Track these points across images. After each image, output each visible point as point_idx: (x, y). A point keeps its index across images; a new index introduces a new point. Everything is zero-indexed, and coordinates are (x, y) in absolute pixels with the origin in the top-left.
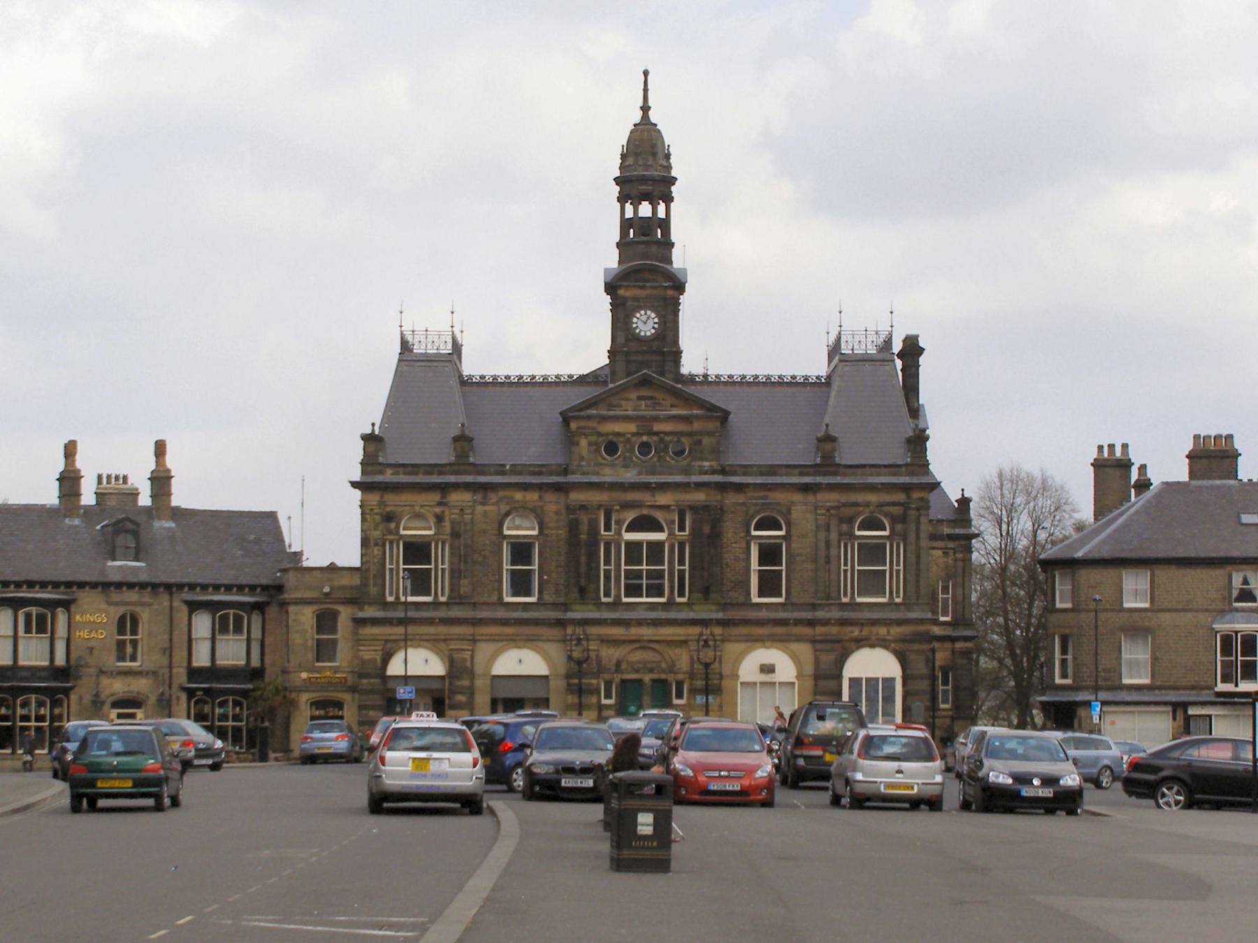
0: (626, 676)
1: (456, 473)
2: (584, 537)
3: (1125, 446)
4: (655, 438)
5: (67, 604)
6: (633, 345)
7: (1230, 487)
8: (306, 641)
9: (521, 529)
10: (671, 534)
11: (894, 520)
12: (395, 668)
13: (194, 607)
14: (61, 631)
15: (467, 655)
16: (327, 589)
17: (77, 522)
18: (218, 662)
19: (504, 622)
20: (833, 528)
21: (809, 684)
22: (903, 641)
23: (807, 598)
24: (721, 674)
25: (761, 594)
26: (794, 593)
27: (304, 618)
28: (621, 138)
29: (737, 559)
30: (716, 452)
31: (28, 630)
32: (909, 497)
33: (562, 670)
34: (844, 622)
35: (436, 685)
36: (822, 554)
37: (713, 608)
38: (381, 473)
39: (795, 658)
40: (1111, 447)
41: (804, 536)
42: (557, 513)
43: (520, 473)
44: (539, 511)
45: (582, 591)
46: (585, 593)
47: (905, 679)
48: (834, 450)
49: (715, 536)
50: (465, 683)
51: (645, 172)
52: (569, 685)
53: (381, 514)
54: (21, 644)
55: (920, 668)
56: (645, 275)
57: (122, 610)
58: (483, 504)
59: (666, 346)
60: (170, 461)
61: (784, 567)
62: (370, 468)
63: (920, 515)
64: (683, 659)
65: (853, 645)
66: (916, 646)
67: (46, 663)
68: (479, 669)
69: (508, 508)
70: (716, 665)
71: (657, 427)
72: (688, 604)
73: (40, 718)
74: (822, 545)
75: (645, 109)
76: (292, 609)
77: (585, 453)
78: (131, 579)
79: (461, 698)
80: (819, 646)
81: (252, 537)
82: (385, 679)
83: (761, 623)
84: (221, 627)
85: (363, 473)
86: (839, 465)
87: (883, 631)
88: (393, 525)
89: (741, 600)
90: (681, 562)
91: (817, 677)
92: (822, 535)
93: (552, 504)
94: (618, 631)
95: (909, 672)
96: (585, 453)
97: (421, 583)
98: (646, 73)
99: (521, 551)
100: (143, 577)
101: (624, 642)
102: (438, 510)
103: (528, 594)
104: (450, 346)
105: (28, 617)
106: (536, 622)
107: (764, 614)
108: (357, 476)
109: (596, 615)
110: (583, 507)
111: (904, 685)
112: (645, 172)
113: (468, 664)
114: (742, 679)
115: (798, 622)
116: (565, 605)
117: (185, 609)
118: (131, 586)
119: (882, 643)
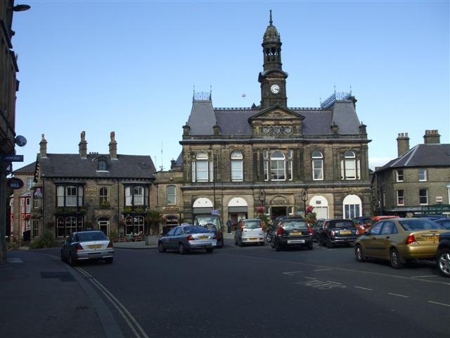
1: (215, 138)
2: (258, 159)
3: (406, 134)
5: (83, 185)
11: (357, 153)
12: (195, 205)
13: (126, 185)
14: (81, 194)
15: (220, 200)
17: (85, 158)
19: (233, 188)
21: (333, 207)
26: (430, 177)
29: (308, 166)
31: (69, 194)
33: (252, 204)
36: (335, 163)
38: (190, 138)
39: (327, 198)
40: (403, 134)
42: (249, 151)
43: (236, 138)
47: (363, 204)
49: (302, 158)
51: (272, 47)
52: (255, 209)
54: (67, 198)
55: (367, 200)
56: (273, 73)
57: (102, 187)
58: (224, 149)
59: (282, 97)
60: (116, 138)
64: (292, 199)
65: (345, 194)
66: (366, 194)
67: (76, 205)
68: (224, 205)
71: (281, 123)
73: (73, 225)
74: (335, 161)
75: (271, 22)
76: (159, 185)
77: (258, 131)
78: (104, 176)
82: (193, 208)
85: (183, 138)
87: (355, 189)
91: (335, 205)
93: (248, 148)
94: (271, 191)
96: (258, 131)
100: (109, 176)
101: (272, 194)
102: (209, 151)
103: (426, 202)
105: (69, 189)
107: (317, 184)
109: (263, 185)
111: (363, 207)
112: (272, 47)
117: (123, 186)
118: (104, 178)
119: (355, 193)
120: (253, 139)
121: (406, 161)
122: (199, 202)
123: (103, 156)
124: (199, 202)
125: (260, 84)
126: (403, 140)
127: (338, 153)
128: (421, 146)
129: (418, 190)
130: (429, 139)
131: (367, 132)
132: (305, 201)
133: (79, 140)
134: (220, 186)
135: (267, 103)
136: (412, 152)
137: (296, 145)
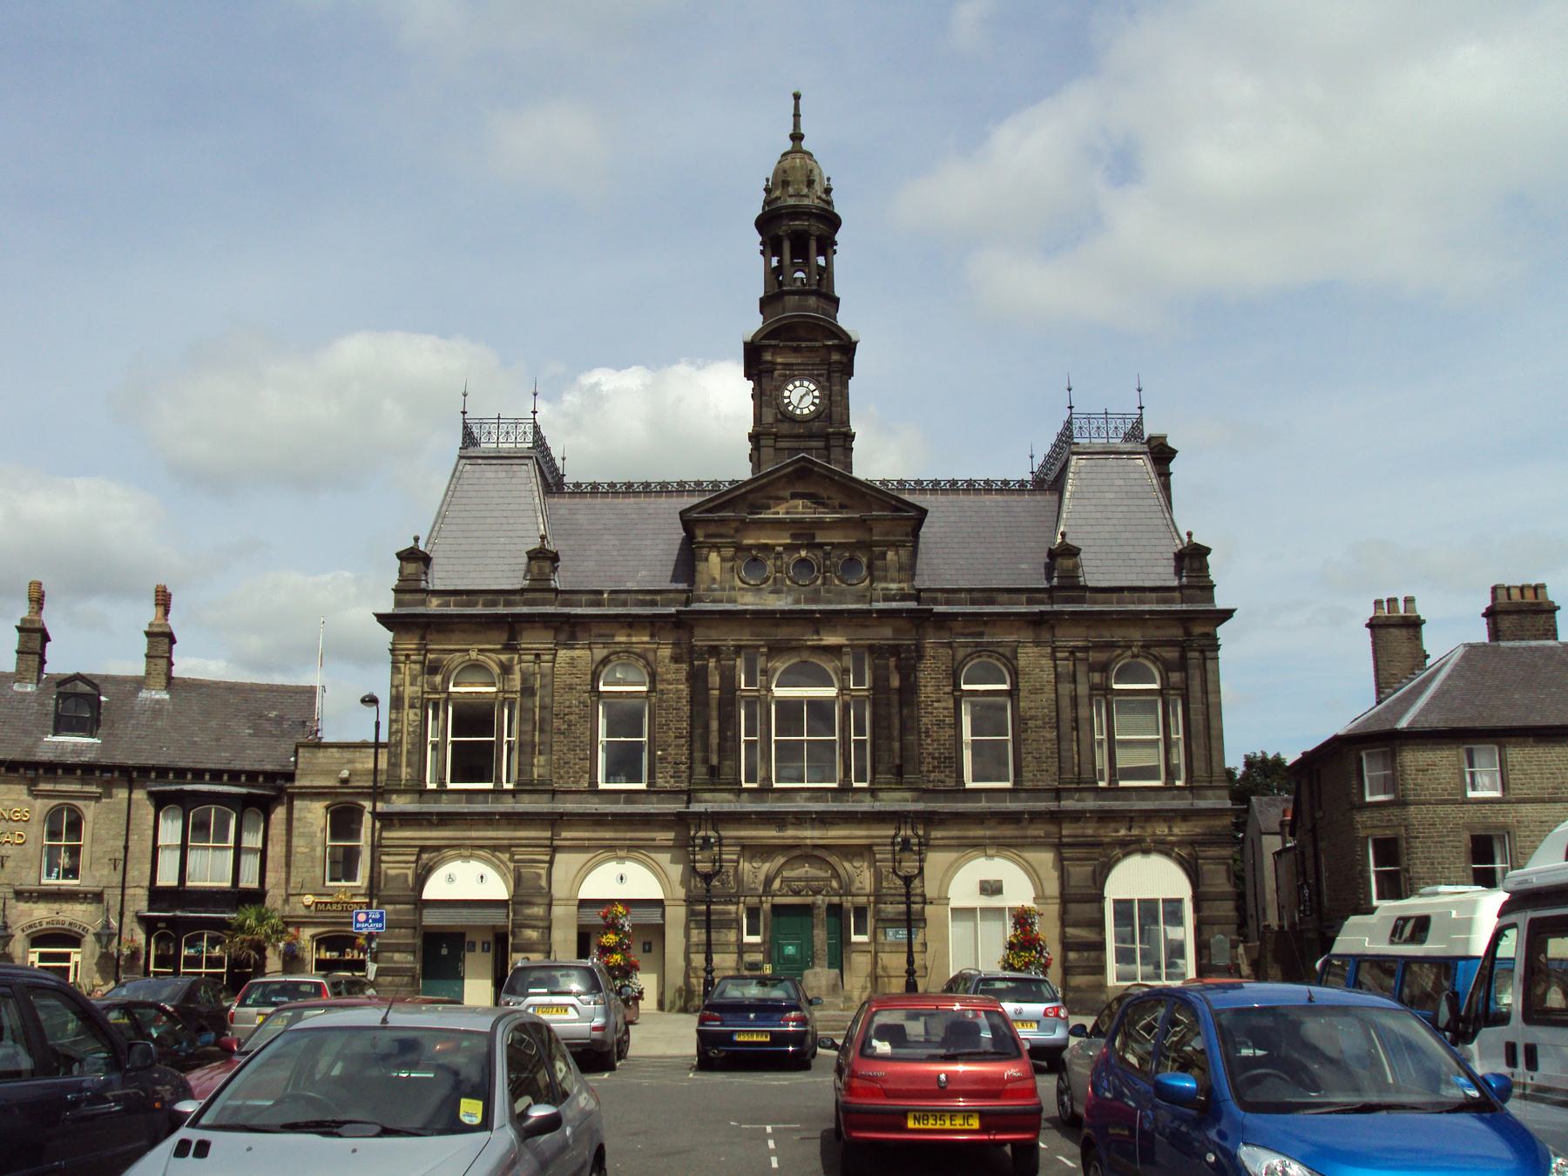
0: (778, 900)
3: (1409, 601)
4: (820, 554)
6: (785, 428)
7: (1551, 648)
8: (313, 849)
9: (626, 684)
10: (843, 689)
11: (1167, 667)
12: (434, 889)
16: (345, 774)
18: (189, 884)
19: (598, 820)
20: (1081, 677)
22: (1192, 843)
23: (1048, 781)
24: (923, 896)
25: (974, 780)
26: (1027, 775)
27: (314, 815)
28: (767, 169)
29: (940, 724)
30: (910, 569)
32: (1188, 633)
34: (1104, 817)
35: (497, 918)
36: (1067, 714)
37: (908, 795)
38: (423, 603)
39: (1032, 872)
40: (1392, 601)
41: (1035, 691)
44: (651, 657)
45: (714, 772)
46: (720, 778)
48: (1076, 567)
49: (909, 690)
50: (539, 911)
51: (798, 228)
53: (422, 663)
55: (1219, 881)
56: (799, 336)
59: (833, 429)
61: (1009, 737)
62: (408, 597)
63: (1205, 659)
65: (1118, 851)
66: (1213, 852)
68: (559, 891)
69: (605, 652)
70: (917, 882)
72: (872, 792)
74: (1065, 703)
75: (797, 137)
77: (716, 573)
79: (533, 934)
80: (1067, 853)
81: (273, 714)
83: (979, 818)
84: (197, 831)
85: (398, 603)
86: (1086, 588)
87: (1161, 830)
88: (438, 679)
89: (950, 783)
90: (860, 730)
92: (1066, 688)
94: (768, 834)
95: (1202, 889)
96: (716, 573)
97: (474, 762)
98: (797, 97)
99: (625, 720)
104: (530, 438)
106: (647, 821)
107: (983, 805)
108: (388, 607)
110: (714, 651)
111: (1197, 908)
112: (798, 228)
113: (544, 883)
114: (953, 904)
115: (1035, 817)
116: (689, 793)
119: (1163, 847)
120: (696, 606)
121: (1406, 710)
122: (450, 879)
123: (1331, 941)
124: (450, 879)
125: (751, 384)
126: (1395, 630)
127: (1082, 670)
128: (1472, 647)
129: (1466, 837)
130: (1506, 623)
131: (1214, 574)
132: (908, 880)
133: (23, 610)
134: (541, 805)
135: (767, 453)
136: (1438, 671)
137: (887, 632)
